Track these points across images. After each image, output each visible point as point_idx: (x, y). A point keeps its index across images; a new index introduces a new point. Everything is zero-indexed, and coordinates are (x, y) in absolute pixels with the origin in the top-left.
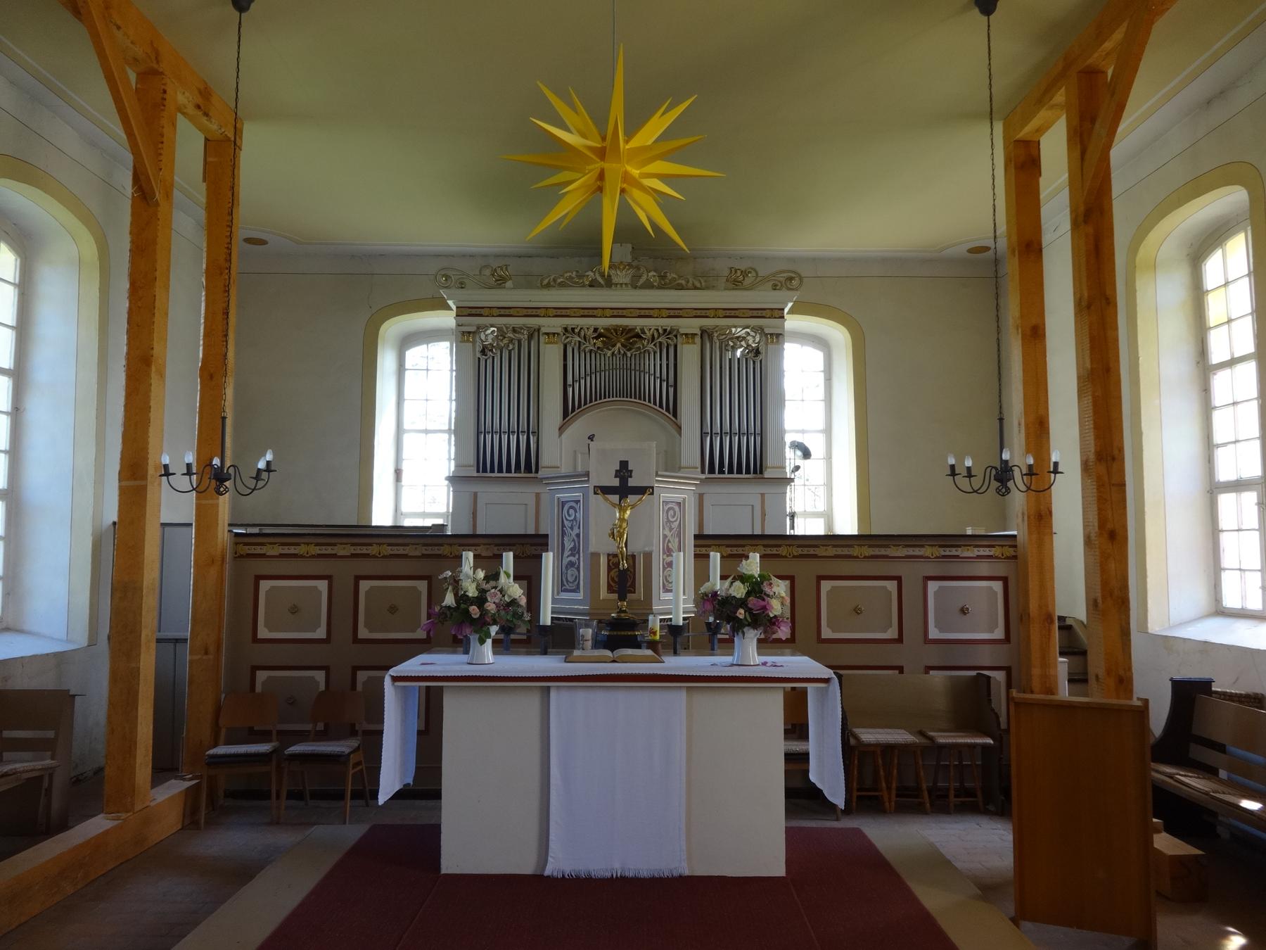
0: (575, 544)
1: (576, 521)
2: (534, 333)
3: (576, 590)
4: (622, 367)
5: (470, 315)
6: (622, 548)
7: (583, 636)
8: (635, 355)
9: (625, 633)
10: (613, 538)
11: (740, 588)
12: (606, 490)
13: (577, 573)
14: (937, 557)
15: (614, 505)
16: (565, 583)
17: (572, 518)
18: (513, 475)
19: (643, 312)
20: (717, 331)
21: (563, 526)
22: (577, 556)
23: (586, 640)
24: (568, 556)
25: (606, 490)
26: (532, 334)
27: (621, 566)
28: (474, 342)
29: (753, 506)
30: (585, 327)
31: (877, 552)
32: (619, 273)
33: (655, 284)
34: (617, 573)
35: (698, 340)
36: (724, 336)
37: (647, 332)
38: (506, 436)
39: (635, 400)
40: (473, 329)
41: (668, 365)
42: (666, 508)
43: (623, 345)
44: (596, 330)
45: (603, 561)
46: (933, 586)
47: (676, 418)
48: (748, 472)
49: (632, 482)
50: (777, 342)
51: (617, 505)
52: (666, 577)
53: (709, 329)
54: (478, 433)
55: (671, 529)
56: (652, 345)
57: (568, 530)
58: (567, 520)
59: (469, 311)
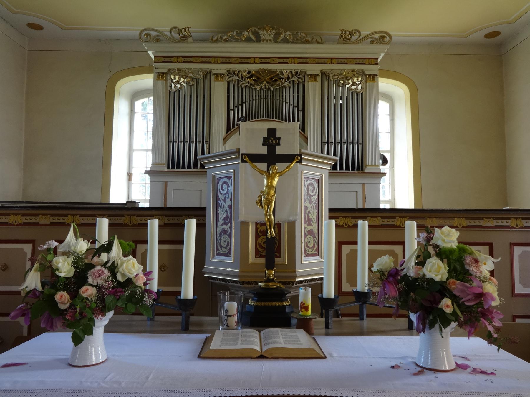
0: (227, 213)
1: (229, 194)
2: (208, 74)
3: (228, 254)
4: (267, 97)
5: (164, 62)
6: (270, 216)
7: (227, 311)
8: (276, 89)
9: (273, 304)
10: (261, 205)
11: (440, 268)
12: (254, 158)
13: (229, 239)
14: (521, 228)
15: (261, 172)
16: (219, 248)
17: (225, 192)
18: (192, 170)
19: (281, 60)
20: (332, 73)
21: (218, 199)
22: (229, 225)
23: (231, 316)
24: (221, 225)
25: (254, 158)
26: (206, 75)
27: (269, 235)
28: (166, 80)
29: (357, 192)
30: (242, 70)
31: (473, 223)
32: (265, 32)
33: (290, 40)
34: (265, 240)
35: (319, 79)
36: (337, 77)
37: (284, 73)
38: (188, 144)
39: (276, 120)
40: (165, 71)
41: (298, 96)
42: (307, 184)
43: (268, 83)
44: (249, 72)
45: (252, 229)
46: (517, 251)
47: (304, 133)
48: (353, 169)
49: (280, 150)
50: (374, 80)
51: (265, 172)
52: (307, 243)
53: (326, 71)
54: (169, 142)
55: (311, 202)
56: (287, 83)
57: (222, 203)
58: (221, 194)
59: (163, 59)
